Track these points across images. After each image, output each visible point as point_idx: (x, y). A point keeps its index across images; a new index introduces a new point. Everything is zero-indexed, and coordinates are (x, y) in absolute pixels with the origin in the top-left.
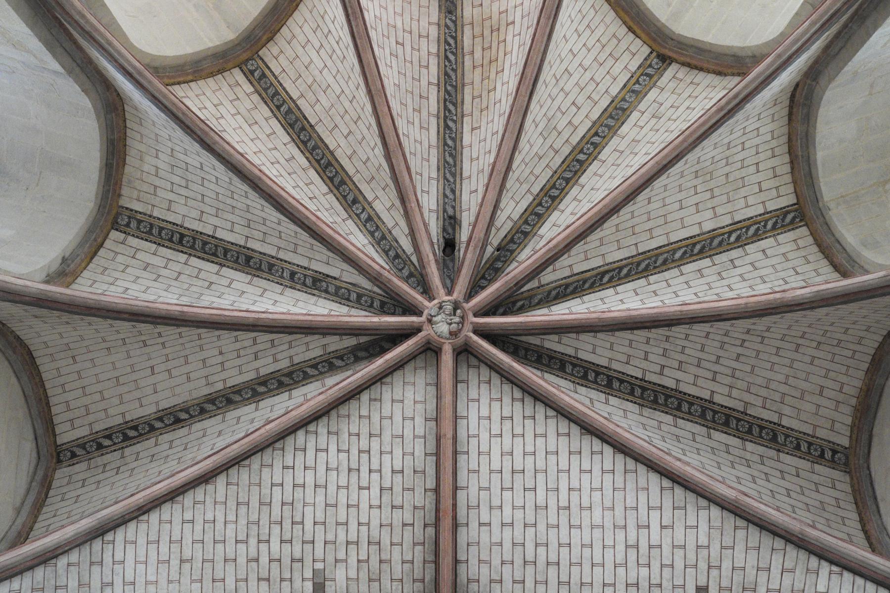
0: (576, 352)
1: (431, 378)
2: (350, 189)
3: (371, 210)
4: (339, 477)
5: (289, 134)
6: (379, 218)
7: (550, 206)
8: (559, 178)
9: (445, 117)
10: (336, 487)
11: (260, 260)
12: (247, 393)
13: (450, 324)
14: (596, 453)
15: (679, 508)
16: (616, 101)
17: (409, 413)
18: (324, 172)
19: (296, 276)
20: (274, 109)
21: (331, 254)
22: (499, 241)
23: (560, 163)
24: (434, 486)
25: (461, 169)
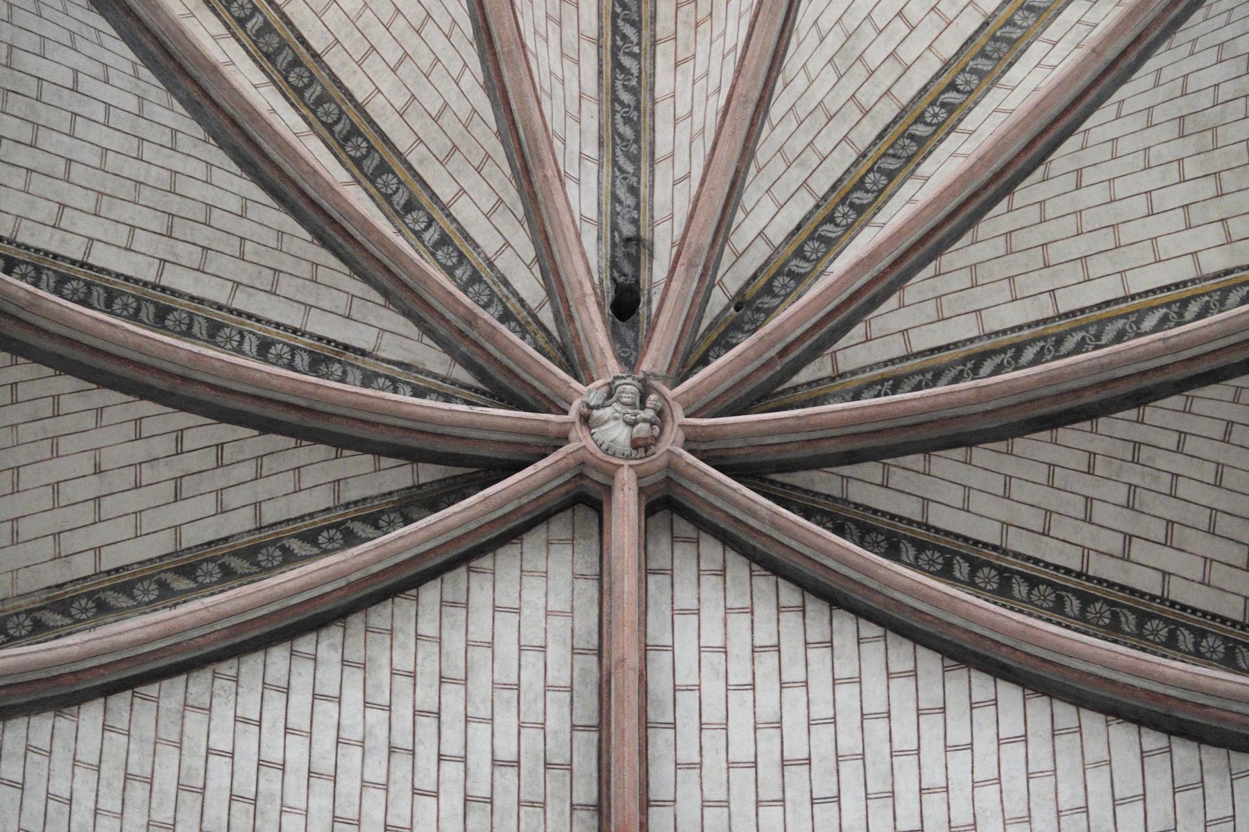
0: (924, 511)
1: (587, 561)
2: (400, 182)
3: (447, 221)
4: (367, 761)
5: (263, 70)
6: (467, 237)
7: (853, 223)
8: (871, 170)
9: (615, 50)
10: (357, 784)
11: (190, 315)
12: (146, 592)
13: (632, 424)
14: (984, 705)
15: (1188, 788)
16: (994, 24)
17: (533, 636)
18: (342, 147)
19: (273, 350)
20: (233, 23)
21: (358, 287)
22: (740, 283)
23: (872, 137)
24: (593, 797)
25: (653, 143)
